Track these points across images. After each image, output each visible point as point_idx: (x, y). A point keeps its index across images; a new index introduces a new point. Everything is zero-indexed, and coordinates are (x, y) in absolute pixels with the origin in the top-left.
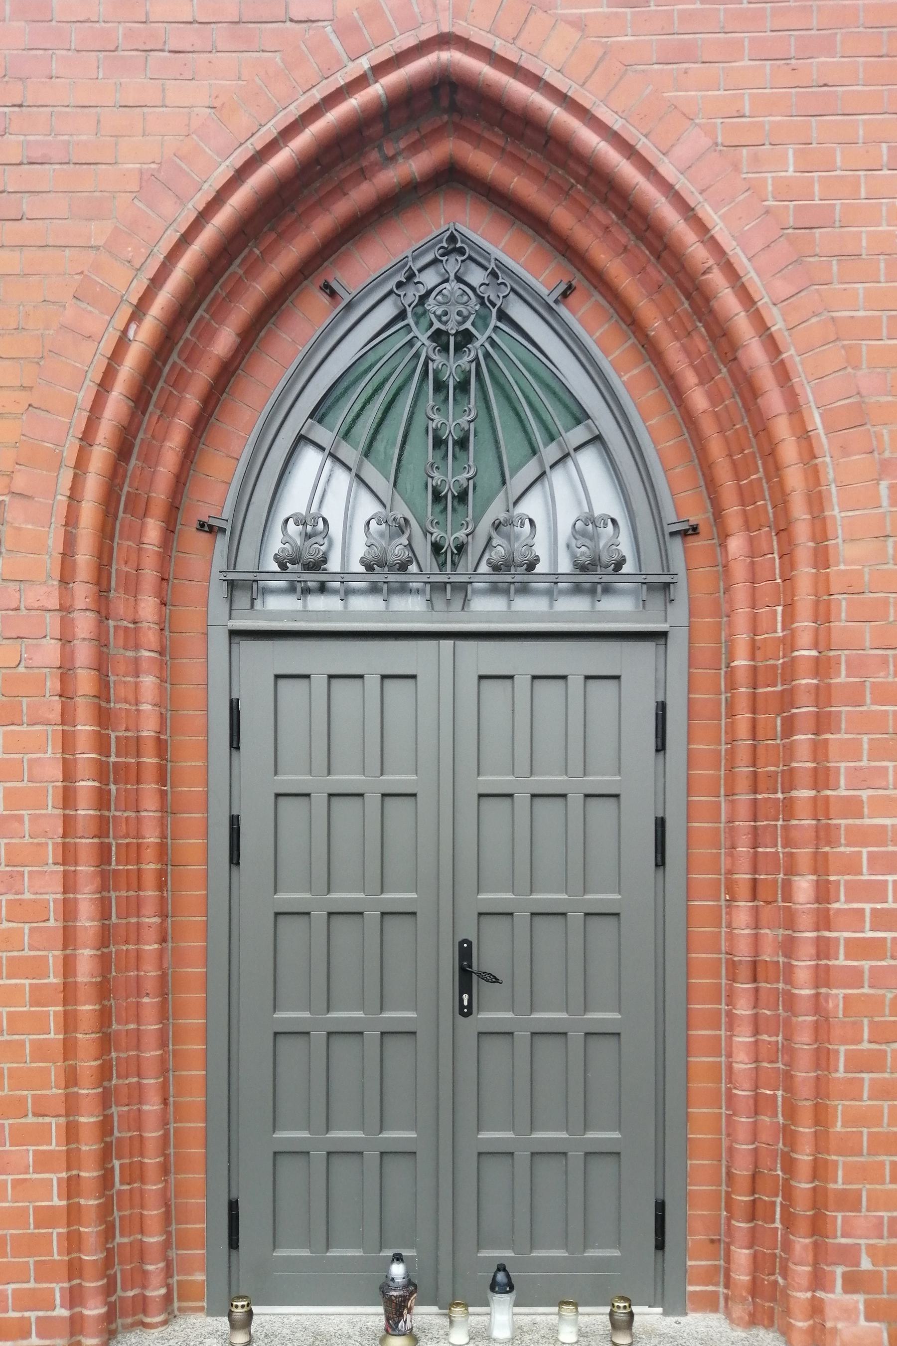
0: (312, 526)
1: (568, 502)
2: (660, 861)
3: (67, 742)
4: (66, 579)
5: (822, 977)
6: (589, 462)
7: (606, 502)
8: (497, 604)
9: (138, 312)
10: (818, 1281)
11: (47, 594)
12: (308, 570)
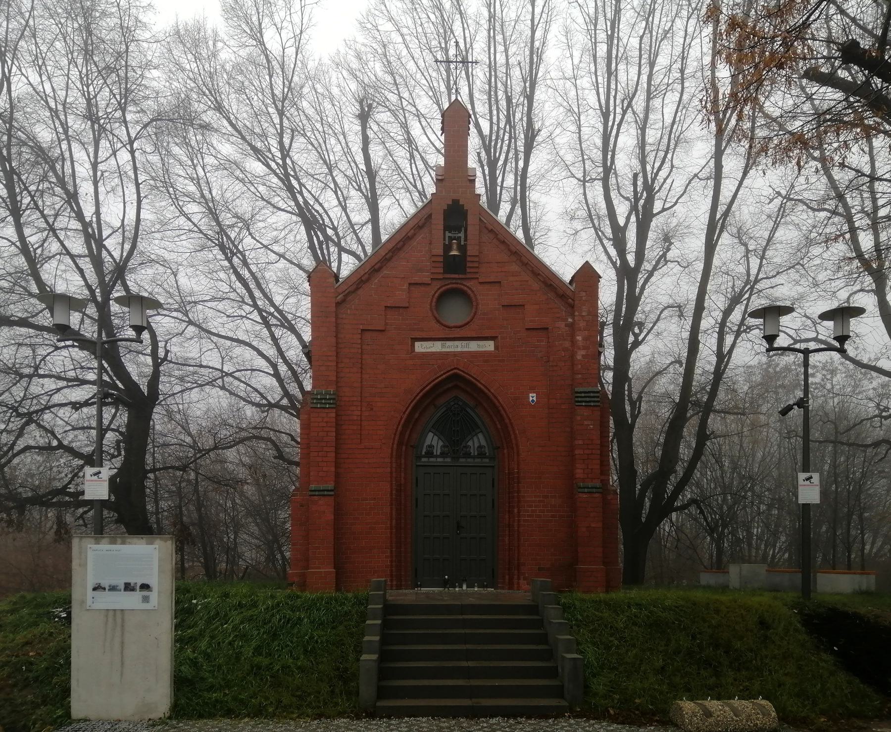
0: (431, 446)
1: (477, 442)
2: (493, 486)
3: (391, 484)
4: (391, 458)
5: (519, 526)
6: (480, 436)
7: (483, 443)
8: (463, 460)
9: (404, 413)
10: (519, 579)
11: (388, 460)
12: (429, 454)
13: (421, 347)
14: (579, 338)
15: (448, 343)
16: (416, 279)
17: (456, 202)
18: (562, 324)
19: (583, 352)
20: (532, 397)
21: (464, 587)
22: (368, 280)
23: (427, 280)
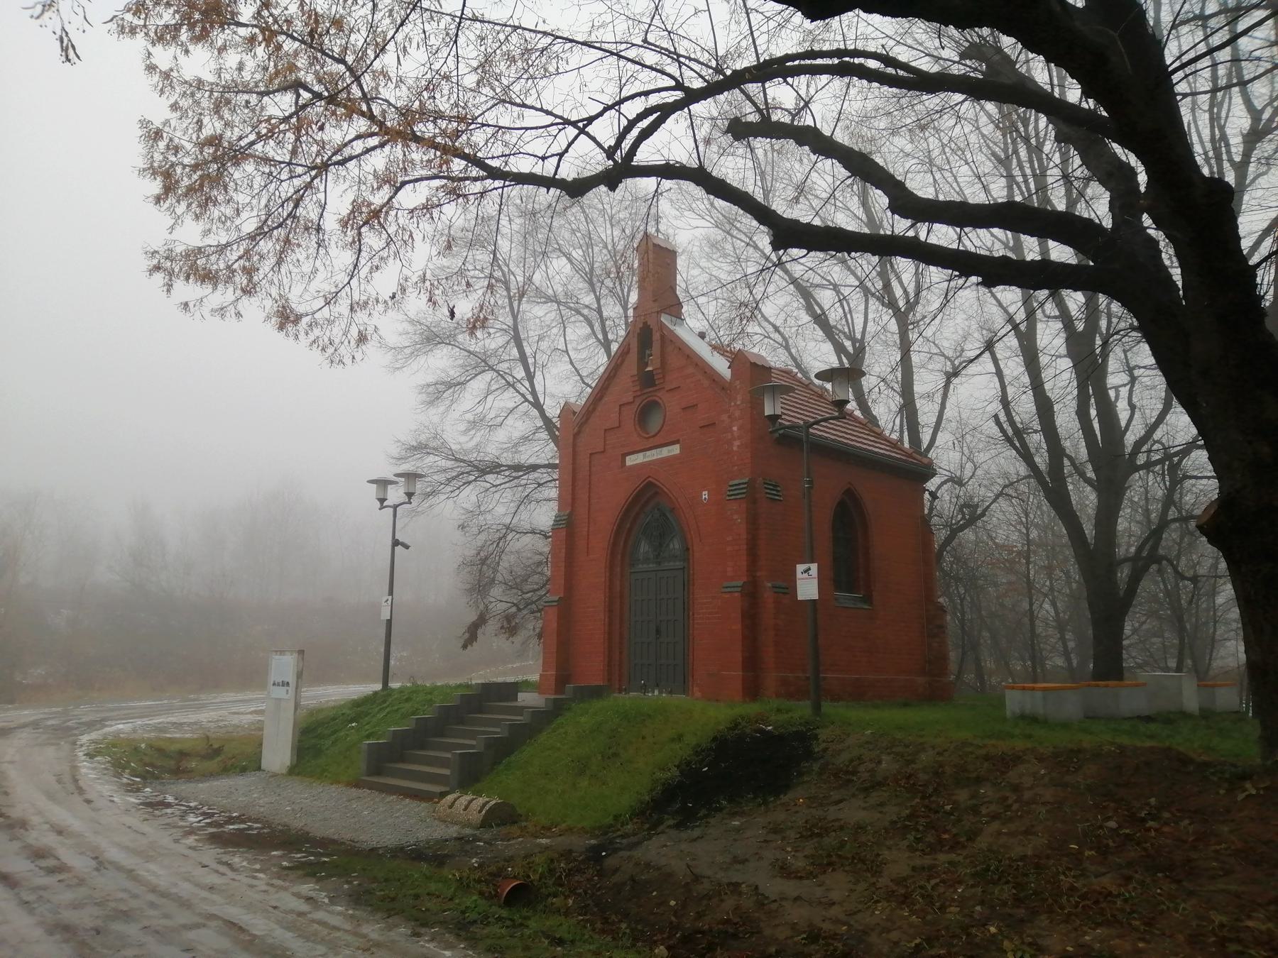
1: (676, 545)
13: (631, 460)
14: (735, 429)
15: (648, 453)
16: (624, 400)
17: (645, 323)
18: (725, 417)
19: (737, 443)
20: (705, 495)
21: (656, 693)
22: (594, 409)
23: (631, 399)
